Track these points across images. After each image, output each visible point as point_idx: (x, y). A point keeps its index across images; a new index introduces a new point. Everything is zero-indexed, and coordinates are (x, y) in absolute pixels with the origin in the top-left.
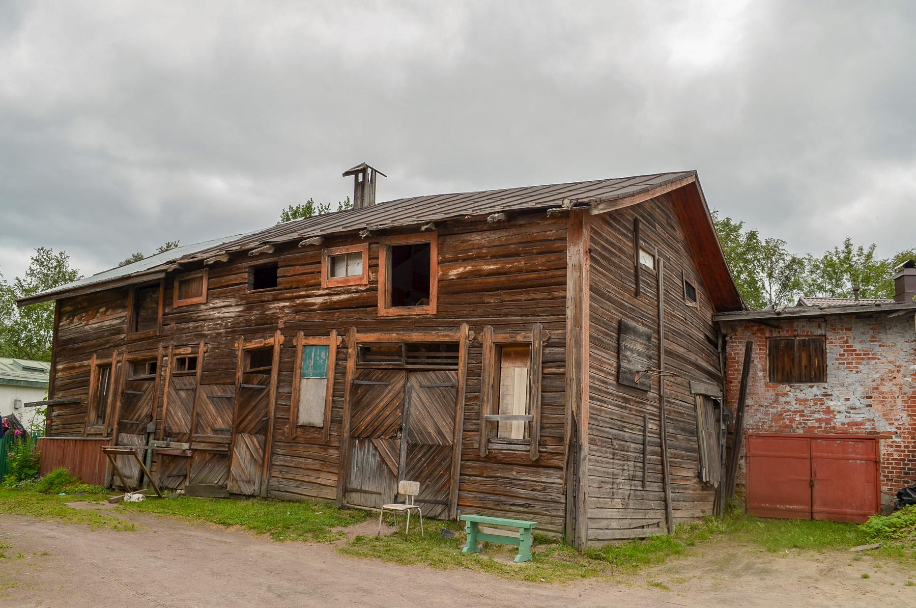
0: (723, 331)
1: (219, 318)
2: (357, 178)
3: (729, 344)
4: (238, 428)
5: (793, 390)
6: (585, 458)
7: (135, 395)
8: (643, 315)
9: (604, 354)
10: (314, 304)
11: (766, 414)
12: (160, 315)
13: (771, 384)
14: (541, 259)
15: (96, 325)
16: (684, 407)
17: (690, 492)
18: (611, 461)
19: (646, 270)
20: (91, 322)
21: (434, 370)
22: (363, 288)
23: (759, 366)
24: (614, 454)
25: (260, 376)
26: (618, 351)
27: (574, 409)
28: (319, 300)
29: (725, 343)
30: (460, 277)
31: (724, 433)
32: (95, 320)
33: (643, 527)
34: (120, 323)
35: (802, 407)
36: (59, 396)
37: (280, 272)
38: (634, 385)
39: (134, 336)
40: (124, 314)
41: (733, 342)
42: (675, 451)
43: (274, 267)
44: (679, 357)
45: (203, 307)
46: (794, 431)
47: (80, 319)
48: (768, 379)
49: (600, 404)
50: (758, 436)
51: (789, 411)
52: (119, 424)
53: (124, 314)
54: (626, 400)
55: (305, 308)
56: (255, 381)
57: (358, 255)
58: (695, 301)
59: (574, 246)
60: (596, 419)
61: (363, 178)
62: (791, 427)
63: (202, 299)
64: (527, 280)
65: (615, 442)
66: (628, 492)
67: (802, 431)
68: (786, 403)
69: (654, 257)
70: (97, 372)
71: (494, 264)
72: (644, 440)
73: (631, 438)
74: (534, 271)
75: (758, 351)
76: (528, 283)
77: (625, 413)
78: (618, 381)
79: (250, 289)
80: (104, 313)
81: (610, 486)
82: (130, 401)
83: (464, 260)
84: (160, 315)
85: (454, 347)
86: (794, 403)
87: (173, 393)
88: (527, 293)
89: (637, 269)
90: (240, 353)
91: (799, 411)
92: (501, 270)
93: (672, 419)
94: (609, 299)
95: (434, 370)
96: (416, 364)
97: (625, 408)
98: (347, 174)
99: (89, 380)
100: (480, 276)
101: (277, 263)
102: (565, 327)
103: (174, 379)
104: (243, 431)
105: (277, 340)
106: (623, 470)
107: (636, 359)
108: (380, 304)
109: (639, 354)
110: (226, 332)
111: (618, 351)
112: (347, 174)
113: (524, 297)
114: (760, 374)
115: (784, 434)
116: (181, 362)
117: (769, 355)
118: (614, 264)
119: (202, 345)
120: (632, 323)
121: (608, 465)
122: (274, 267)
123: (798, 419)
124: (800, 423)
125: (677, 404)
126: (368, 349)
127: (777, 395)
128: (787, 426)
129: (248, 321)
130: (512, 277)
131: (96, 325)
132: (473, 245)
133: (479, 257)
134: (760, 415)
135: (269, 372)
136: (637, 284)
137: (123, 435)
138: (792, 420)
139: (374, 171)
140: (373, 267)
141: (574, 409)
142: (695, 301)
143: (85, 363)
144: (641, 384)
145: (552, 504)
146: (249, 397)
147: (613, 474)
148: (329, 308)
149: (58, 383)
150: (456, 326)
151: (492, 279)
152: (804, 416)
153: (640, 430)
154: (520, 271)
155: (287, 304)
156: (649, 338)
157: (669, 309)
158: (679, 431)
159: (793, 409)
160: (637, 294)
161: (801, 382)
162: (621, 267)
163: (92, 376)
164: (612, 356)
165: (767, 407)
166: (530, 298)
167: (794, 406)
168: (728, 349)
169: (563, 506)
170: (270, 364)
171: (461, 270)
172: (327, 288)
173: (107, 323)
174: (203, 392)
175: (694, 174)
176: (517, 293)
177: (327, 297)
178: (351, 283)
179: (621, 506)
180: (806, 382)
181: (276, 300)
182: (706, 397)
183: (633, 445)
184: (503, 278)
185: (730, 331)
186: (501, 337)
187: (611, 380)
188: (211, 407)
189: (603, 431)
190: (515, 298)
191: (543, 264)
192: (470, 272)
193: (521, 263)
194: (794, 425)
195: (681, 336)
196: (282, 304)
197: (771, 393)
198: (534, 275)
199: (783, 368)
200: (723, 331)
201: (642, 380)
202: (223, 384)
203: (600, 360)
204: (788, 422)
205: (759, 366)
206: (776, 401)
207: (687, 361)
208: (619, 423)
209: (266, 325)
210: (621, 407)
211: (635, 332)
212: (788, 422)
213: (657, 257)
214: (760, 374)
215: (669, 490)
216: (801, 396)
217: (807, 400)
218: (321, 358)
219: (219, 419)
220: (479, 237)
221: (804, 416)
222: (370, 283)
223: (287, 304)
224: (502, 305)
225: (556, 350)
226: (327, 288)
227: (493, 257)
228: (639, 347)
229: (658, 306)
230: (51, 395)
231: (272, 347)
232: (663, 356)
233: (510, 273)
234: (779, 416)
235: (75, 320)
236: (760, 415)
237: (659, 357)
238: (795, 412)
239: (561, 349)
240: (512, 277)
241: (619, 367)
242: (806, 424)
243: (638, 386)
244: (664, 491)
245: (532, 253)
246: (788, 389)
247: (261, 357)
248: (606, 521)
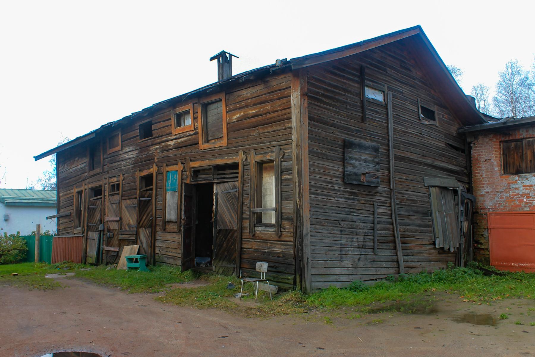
0: (469, 140)
1: (128, 159)
2: (219, 61)
3: (473, 149)
4: (139, 225)
5: (520, 179)
6: (307, 234)
7: (94, 208)
8: (371, 134)
9: (328, 164)
10: (170, 145)
11: (501, 198)
12: (102, 160)
13: (504, 176)
14: (279, 103)
15: (74, 169)
16: (416, 196)
17: (426, 255)
18: (340, 236)
19: (374, 103)
20: (72, 166)
21: (227, 182)
22: (192, 133)
23: (495, 163)
24: (341, 231)
25: (148, 192)
26: (343, 160)
27: (298, 202)
28: (172, 143)
29: (470, 148)
30: (239, 120)
31: (462, 214)
32: (74, 166)
33: (376, 280)
34: (85, 166)
35: (528, 191)
36: (63, 212)
37: (153, 127)
38: (361, 183)
39: (92, 173)
40: (86, 160)
41: (476, 147)
42: (408, 227)
43: (150, 124)
44: (413, 161)
45: (121, 152)
46: (523, 209)
47: (67, 166)
48: (502, 172)
49: (325, 197)
50: (496, 214)
51: (518, 194)
52: (88, 226)
53: (86, 160)
54: (352, 194)
55: (167, 149)
56: (146, 196)
57: (187, 113)
58: (434, 120)
59: (295, 91)
60: (322, 208)
61: (224, 60)
62: (520, 206)
63: (119, 148)
64: (273, 118)
65: (342, 223)
66: (358, 257)
67: (528, 209)
68: (515, 188)
69: (384, 92)
70: (77, 196)
71: (255, 109)
72: (374, 221)
73: (360, 219)
74: (276, 111)
75: (494, 152)
76: (273, 120)
77: (352, 202)
78: (343, 181)
79: (140, 139)
80: (78, 161)
81: (339, 253)
82: (91, 212)
83: (240, 109)
84: (102, 160)
85: (235, 166)
86: (522, 188)
87: (110, 206)
88: (272, 126)
89: (364, 103)
90: (138, 179)
91: (525, 194)
92: (259, 113)
93: (405, 205)
94: (333, 125)
95: (227, 182)
96: (224, 178)
97: (353, 199)
98: (212, 59)
99: (73, 202)
100: (248, 118)
101: (151, 121)
102: (291, 148)
103: (110, 197)
104: (141, 227)
105: (154, 170)
106: (352, 241)
107: (362, 164)
108: (200, 142)
109: (365, 161)
110: (132, 167)
111: (343, 160)
112: (212, 59)
113: (271, 129)
114: (496, 169)
115: (515, 212)
116: (113, 186)
117: (503, 154)
118: (338, 100)
119: (121, 175)
120: (356, 140)
121: (335, 239)
122: (150, 124)
123: (525, 200)
124: (527, 203)
125: (410, 195)
126: (199, 171)
127: (509, 183)
128: (517, 206)
129: (142, 158)
130: (268, 116)
131: (74, 169)
132: (243, 98)
133: (247, 106)
134: (497, 199)
135: (151, 189)
136: (363, 112)
137: (90, 233)
138: (521, 201)
139: (231, 55)
140: (195, 119)
141: (298, 202)
142: (434, 120)
143: (71, 191)
144: (368, 182)
145: (288, 266)
146: (143, 207)
147: (341, 244)
148: (178, 147)
149: (61, 204)
150: (236, 152)
151: (254, 120)
152: (530, 197)
153: (370, 214)
154: (268, 113)
155: (158, 146)
156: (376, 150)
157: (400, 128)
158: (412, 213)
159: (521, 193)
160: (363, 119)
161: (527, 172)
162: (346, 103)
163: (75, 200)
164: (338, 165)
165: (501, 192)
166: (274, 130)
167: (522, 191)
168: (473, 152)
169: (294, 267)
170: (152, 185)
171: (238, 115)
172: (175, 135)
173: (79, 167)
174: (124, 204)
175: (419, 27)
176: (266, 127)
177: (176, 141)
178: (186, 130)
179: (351, 266)
180: (531, 172)
181: (153, 145)
182: (443, 189)
183: (362, 224)
184: (260, 118)
185: (473, 139)
186: (259, 158)
187: (338, 181)
188: (127, 213)
189: (329, 216)
190: (266, 131)
191: (280, 106)
192: (243, 116)
193: (268, 107)
194: (523, 205)
195: (414, 146)
196: (156, 147)
197: (504, 182)
198: (275, 114)
199: (514, 163)
200: (469, 140)
201: (368, 179)
202: (132, 199)
203: (324, 168)
204: (518, 203)
205: (495, 163)
206: (509, 187)
207: (420, 163)
208: (346, 210)
209: (149, 161)
210: (349, 199)
211: (361, 146)
212: (518, 203)
213: (386, 92)
214: (496, 169)
215: (400, 254)
216: (527, 183)
217: (531, 186)
218: (174, 179)
219: (130, 218)
220: (246, 92)
221: (530, 197)
222: (195, 129)
223: (158, 146)
224: (260, 136)
225: (288, 163)
226: (175, 135)
227: (254, 105)
228: (366, 157)
229: (388, 127)
230: (58, 212)
231: (152, 174)
232: (392, 162)
233: (264, 114)
234: (511, 198)
235: (65, 166)
236: (497, 199)
237: (389, 162)
238: (523, 195)
239: (291, 162)
240: (264, 117)
241: (344, 172)
242: (531, 203)
243: (366, 184)
244: (397, 255)
245: (274, 100)
246: (517, 178)
247: (148, 180)
248: (335, 276)
